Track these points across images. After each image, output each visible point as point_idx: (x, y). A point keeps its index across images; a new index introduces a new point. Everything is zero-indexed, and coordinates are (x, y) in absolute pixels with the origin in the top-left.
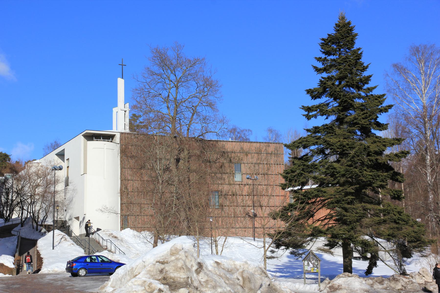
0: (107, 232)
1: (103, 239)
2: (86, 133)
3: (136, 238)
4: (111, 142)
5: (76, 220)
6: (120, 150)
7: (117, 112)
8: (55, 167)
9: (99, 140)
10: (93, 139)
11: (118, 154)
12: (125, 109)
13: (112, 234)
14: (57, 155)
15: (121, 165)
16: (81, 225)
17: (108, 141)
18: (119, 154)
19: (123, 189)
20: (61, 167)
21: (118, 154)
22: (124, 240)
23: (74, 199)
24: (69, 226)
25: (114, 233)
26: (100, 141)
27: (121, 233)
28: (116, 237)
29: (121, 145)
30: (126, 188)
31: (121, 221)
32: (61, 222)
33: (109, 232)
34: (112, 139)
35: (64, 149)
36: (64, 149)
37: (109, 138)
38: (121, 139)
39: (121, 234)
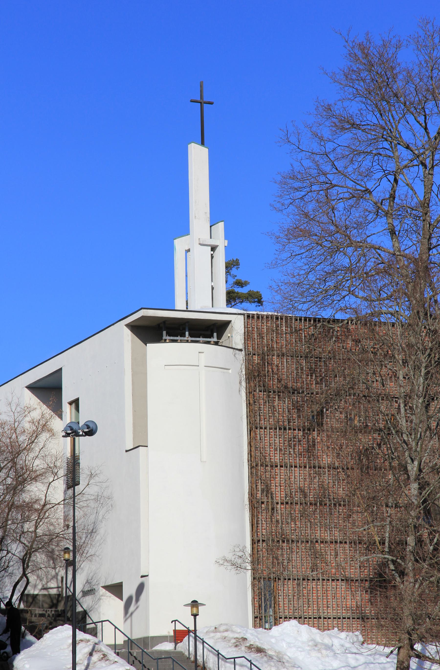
0: (226, 634)
1: (219, 654)
2: (143, 317)
3: (324, 652)
4: (216, 343)
5: (108, 594)
6: (247, 369)
7: (188, 251)
8: (75, 427)
9: (179, 338)
10: (162, 336)
11: (240, 383)
12: (213, 242)
13: (245, 639)
14: (32, 388)
15: (248, 417)
16: (132, 608)
17: (208, 343)
18: (244, 384)
19: (259, 495)
20: (91, 425)
21: (240, 383)
22: (287, 658)
23: (102, 529)
24: (85, 614)
25: (248, 636)
26: (181, 341)
27: (272, 637)
28: (259, 650)
29: (248, 354)
30: (267, 490)
31: (253, 598)
32: (48, 601)
33: (233, 631)
34: (219, 337)
35: (61, 369)
36: (61, 369)
37: (209, 333)
38: (248, 336)
39: (273, 641)
